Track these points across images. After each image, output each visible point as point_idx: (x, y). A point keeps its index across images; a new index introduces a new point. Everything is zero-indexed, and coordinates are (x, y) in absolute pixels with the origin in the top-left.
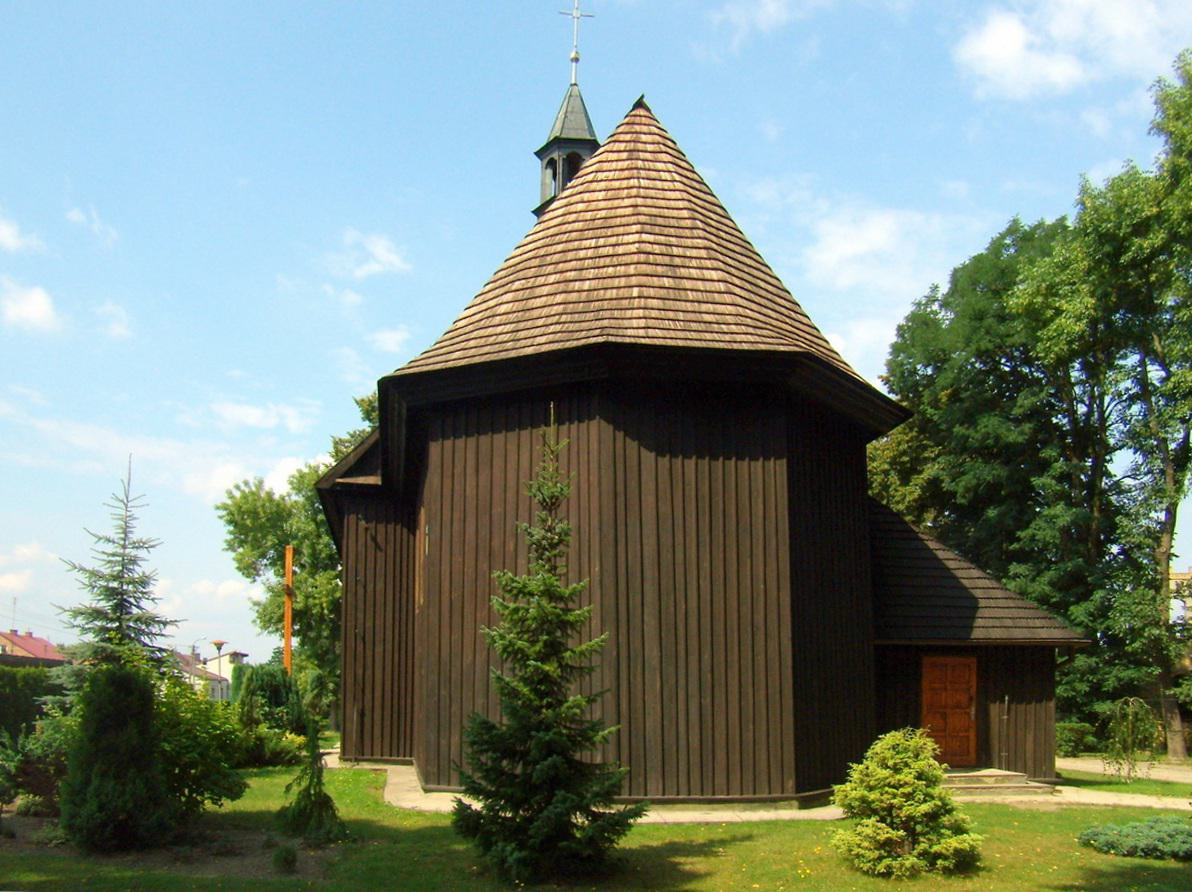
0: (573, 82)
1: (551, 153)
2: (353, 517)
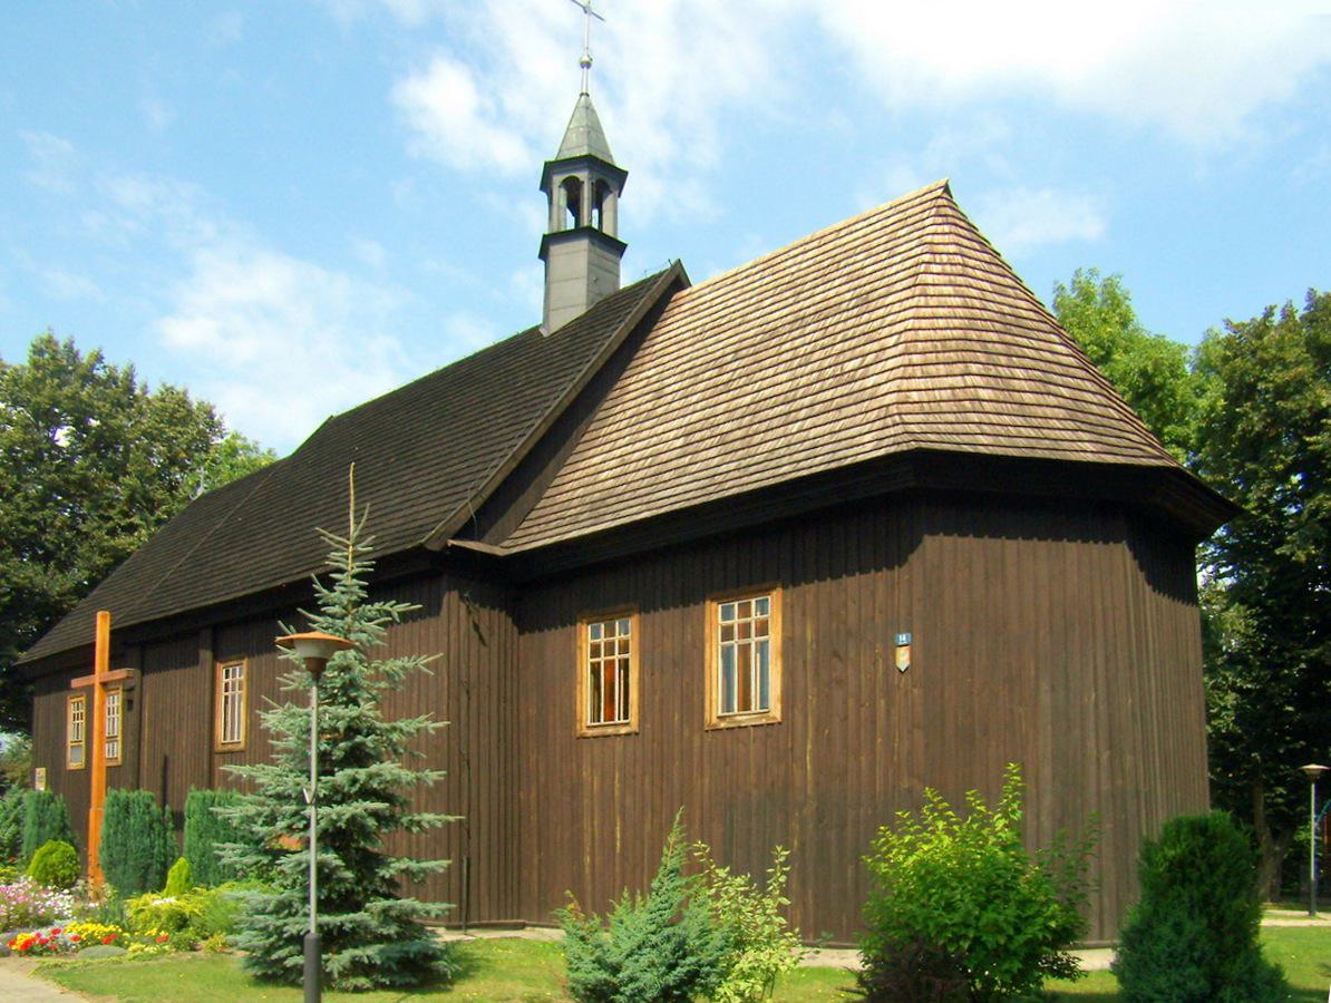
0: (584, 91)
1: (575, 170)
2: (455, 594)
